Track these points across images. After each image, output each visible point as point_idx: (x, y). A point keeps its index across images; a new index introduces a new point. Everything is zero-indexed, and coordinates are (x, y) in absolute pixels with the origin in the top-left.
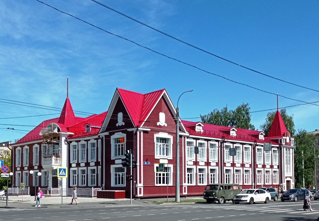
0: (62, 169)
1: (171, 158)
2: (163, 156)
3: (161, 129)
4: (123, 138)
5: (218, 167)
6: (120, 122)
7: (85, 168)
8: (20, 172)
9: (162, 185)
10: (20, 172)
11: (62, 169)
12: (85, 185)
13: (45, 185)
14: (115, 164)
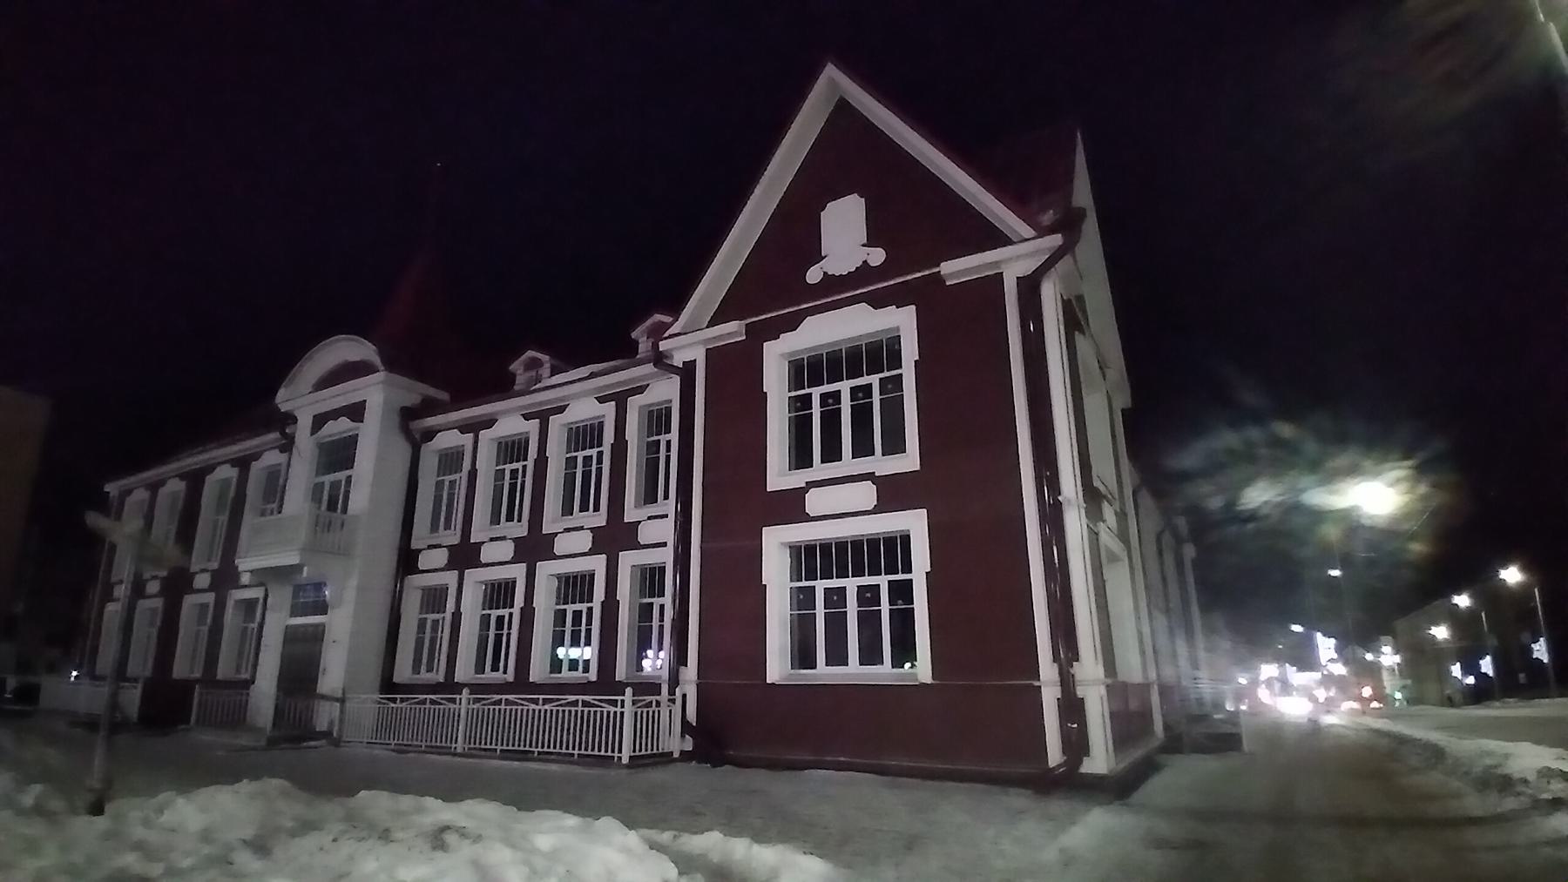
9: (854, 671)
10: (210, 598)
12: (510, 677)
13: (238, 671)
14: (637, 546)
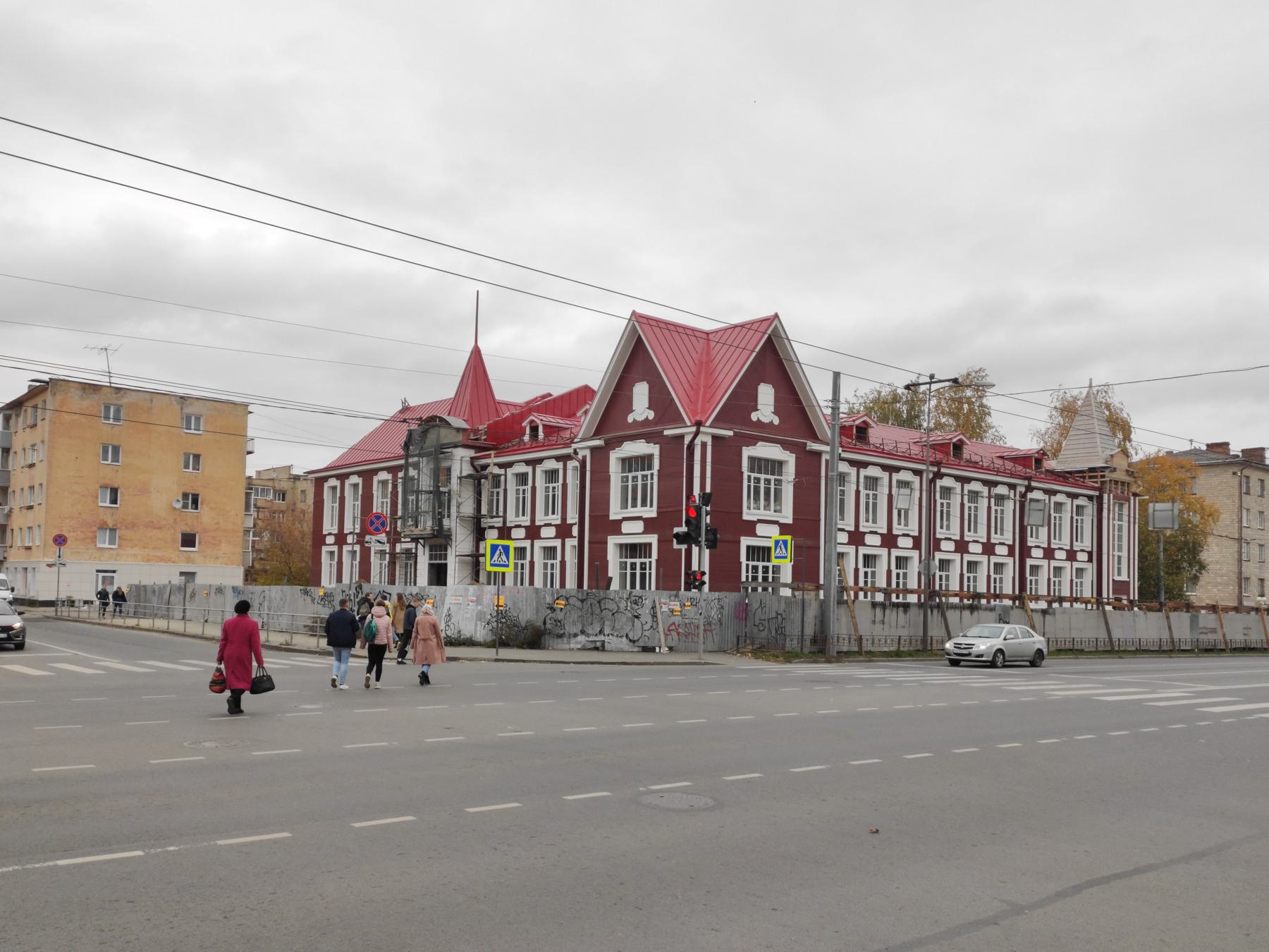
0: (500, 547)
1: (790, 521)
2: (553, 516)
3: (764, 433)
4: (650, 457)
5: (918, 551)
6: (641, 406)
7: (527, 544)
8: (335, 548)
11: (500, 547)
